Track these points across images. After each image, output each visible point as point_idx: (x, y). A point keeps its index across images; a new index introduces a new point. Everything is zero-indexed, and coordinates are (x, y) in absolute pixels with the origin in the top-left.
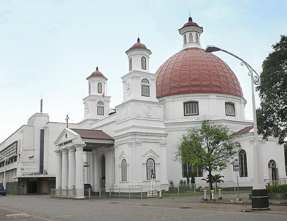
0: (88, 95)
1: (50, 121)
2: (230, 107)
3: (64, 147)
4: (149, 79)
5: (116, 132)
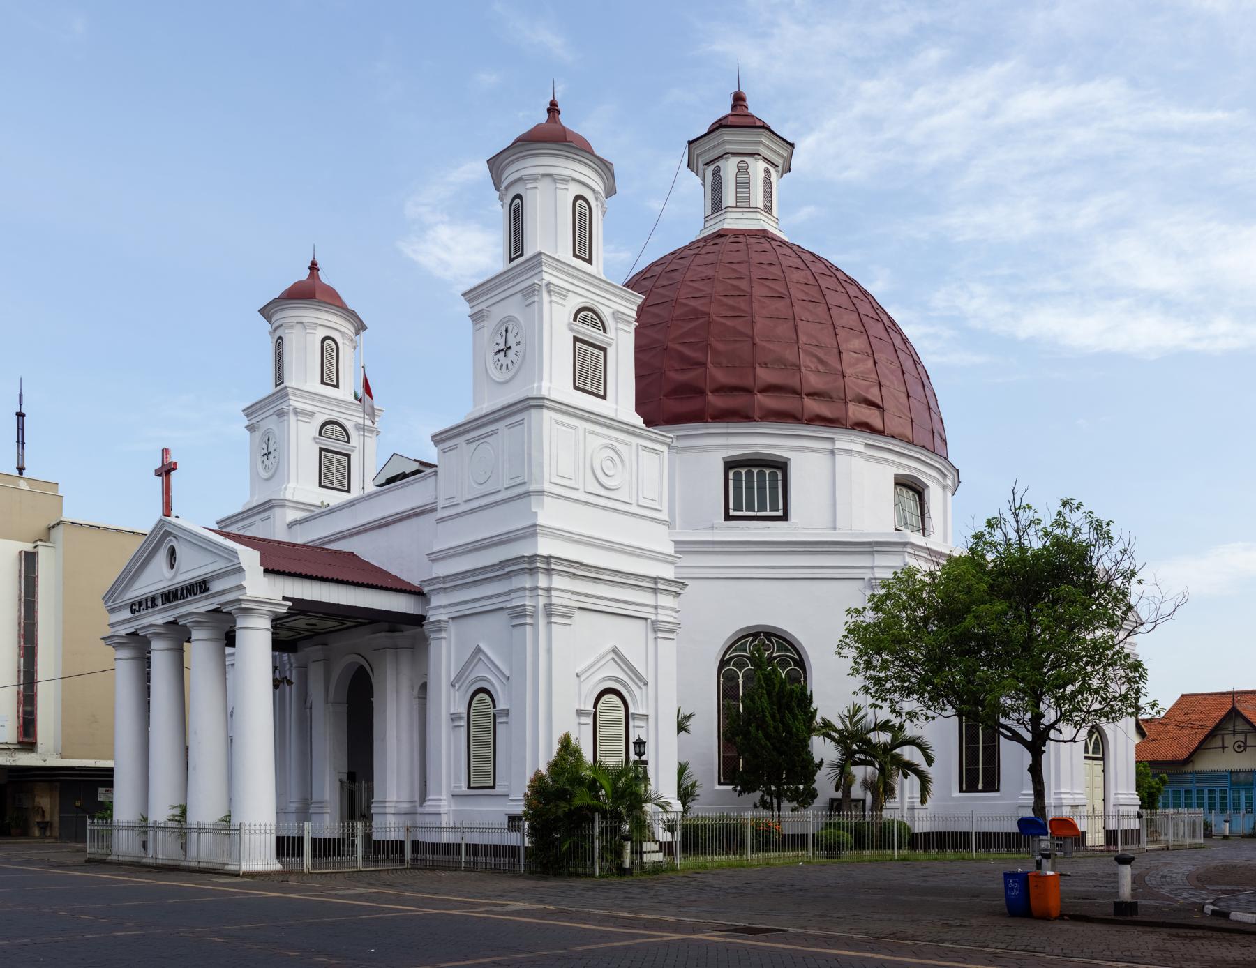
0: (271, 389)
1: (67, 516)
2: (909, 498)
3: (157, 618)
4: (606, 313)
5: (435, 558)
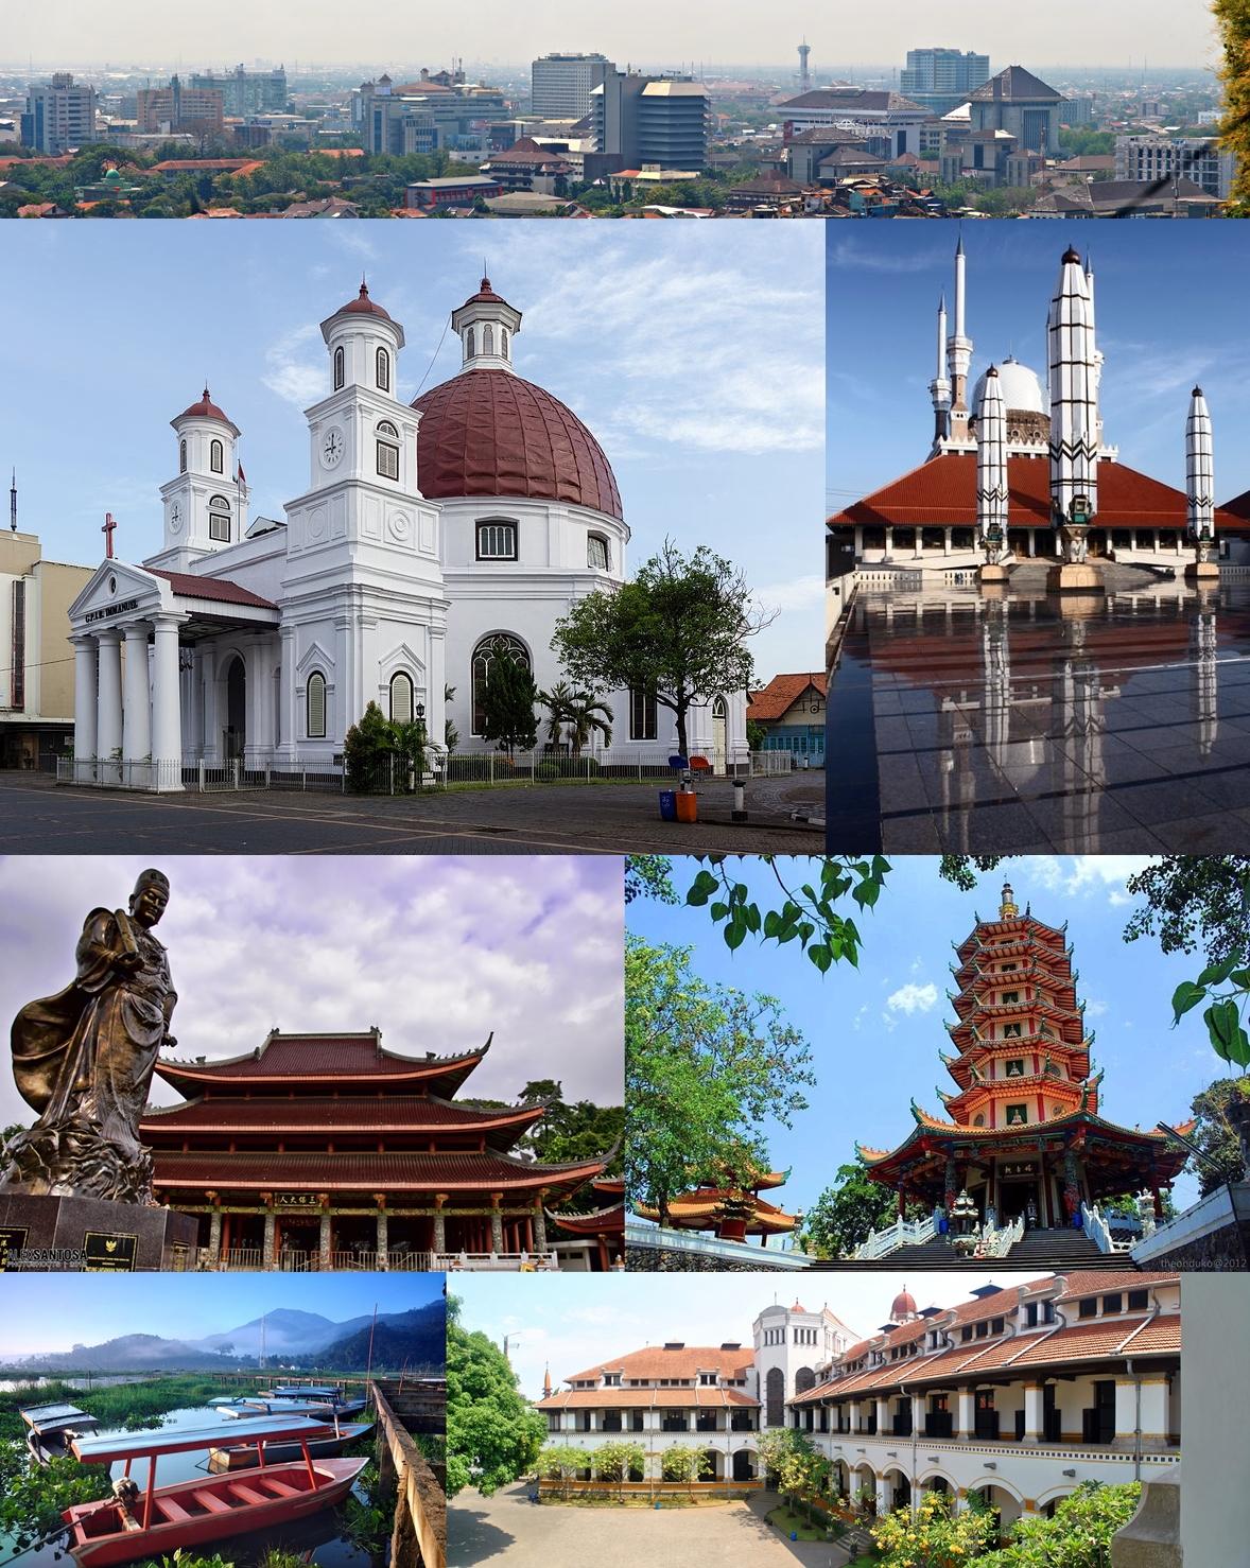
5: (286, 585)
